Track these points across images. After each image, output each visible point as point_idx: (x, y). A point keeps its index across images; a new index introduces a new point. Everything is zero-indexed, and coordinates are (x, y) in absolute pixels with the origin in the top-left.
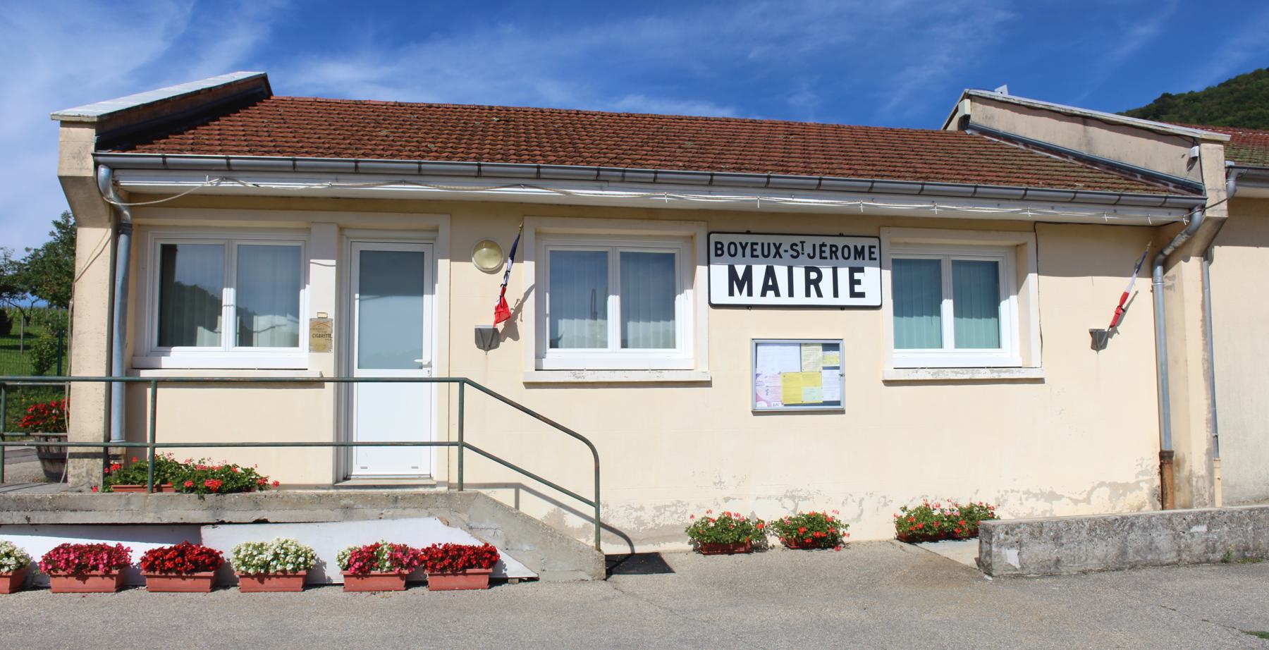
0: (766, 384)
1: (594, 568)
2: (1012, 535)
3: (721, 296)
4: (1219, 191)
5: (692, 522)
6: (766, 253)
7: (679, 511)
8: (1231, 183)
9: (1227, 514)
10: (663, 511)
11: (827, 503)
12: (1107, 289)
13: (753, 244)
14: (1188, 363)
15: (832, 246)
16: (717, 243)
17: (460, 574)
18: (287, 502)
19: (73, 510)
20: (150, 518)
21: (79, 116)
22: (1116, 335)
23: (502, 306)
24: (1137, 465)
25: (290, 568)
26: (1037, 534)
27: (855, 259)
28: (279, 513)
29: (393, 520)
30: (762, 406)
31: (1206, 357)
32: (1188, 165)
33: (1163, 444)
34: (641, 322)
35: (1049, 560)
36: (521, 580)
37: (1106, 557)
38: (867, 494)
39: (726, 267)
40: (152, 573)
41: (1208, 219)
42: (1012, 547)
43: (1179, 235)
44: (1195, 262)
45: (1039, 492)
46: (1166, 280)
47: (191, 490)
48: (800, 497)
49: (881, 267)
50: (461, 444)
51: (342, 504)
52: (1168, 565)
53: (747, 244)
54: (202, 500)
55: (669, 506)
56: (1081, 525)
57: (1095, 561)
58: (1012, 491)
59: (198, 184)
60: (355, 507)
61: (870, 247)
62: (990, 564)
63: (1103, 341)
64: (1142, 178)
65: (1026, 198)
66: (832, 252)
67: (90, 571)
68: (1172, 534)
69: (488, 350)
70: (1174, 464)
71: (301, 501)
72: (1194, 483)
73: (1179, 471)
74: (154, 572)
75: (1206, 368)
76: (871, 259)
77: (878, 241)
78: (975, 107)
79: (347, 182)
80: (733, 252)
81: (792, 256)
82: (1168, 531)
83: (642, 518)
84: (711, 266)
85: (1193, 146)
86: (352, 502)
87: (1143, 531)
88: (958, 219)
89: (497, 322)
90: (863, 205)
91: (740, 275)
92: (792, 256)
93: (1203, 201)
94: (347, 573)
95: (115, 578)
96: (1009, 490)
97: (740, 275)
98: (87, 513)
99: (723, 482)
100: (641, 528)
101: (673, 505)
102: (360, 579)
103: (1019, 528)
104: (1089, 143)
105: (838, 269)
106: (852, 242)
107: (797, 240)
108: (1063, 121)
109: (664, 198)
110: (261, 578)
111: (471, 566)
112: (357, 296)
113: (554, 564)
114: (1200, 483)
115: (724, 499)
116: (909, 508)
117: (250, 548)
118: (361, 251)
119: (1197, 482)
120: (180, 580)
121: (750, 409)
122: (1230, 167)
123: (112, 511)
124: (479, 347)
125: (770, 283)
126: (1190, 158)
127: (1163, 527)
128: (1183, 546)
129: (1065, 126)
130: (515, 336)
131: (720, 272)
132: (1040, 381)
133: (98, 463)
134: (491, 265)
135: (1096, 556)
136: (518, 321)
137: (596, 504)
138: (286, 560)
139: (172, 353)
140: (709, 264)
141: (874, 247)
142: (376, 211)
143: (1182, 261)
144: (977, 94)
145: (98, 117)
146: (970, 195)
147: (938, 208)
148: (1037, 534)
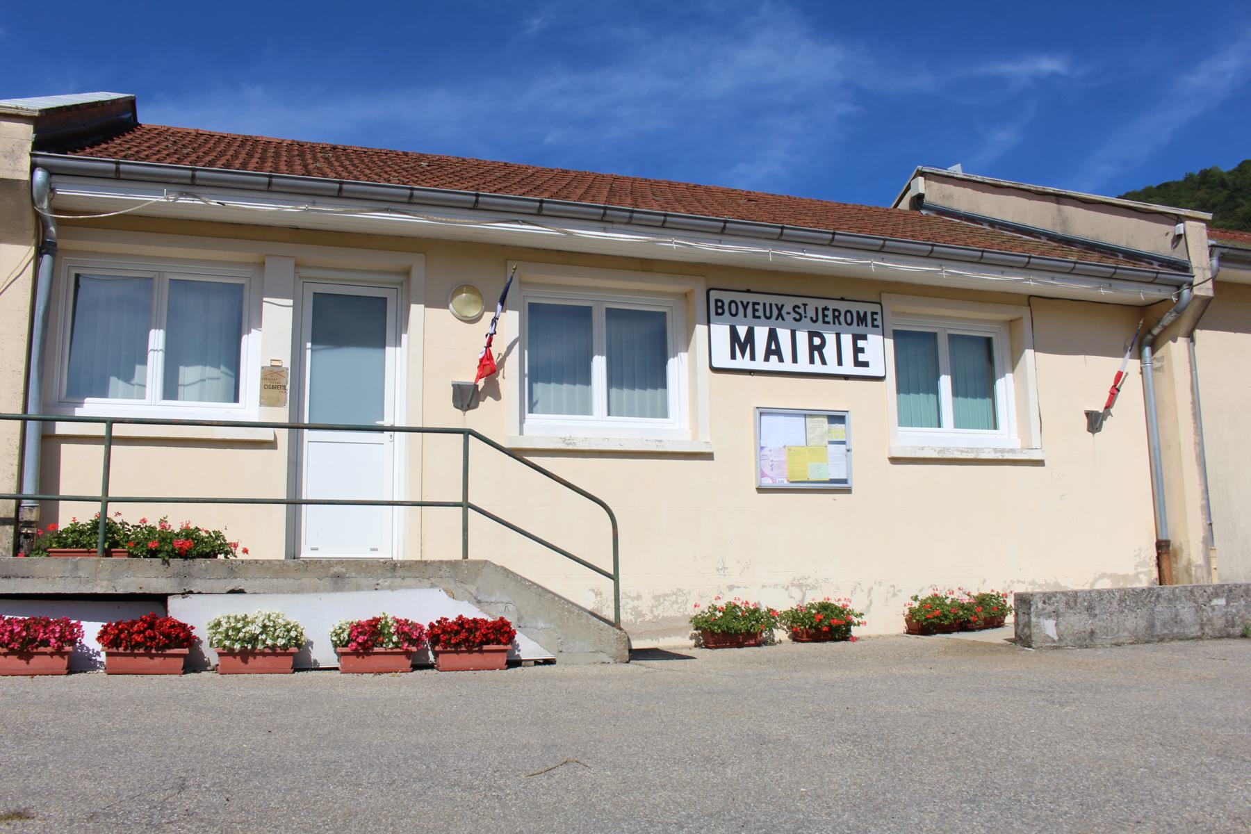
0: (771, 459)
1: (616, 648)
2: (1049, 605)
3: (722, 358)
4: (1204, 269)
5: (698, 611)
6: (768, 315)
7: (680, 601)
8: (1215, 262)
9: (1243, 588)
10: (662, 600)
11: (835, 592)
12: (1101, 368)
13: (754, 304)
14: (1182, 447)
15: (834, 310)
16: (717, 301)
17: (476, 651)
18: (268, 569)
19: (6, 577)
20: (102, 587)
21: (17, 108)
22: (1109, 417)
23: (488, 357)
24: (1136, 556)
25: (282, 643)
26: (1072, 604)
27: (858, 325)
28: (258, 582)
29: (393, 590)
30: (767, 482)
31: (1197, 441)
32: (1173, 243)
33: (1159, 532)
34: (625, 390)
35: (1084, 632)
36: (537, 663)
37: (1136, 629)
38: (875, 582)
39: (727, 328)
40: (114, 650)
41: (1196, 297)
42: (1050, 617)
43: (1168, 314)
44: (1182, 342)
45: (1044, 583)
46: (1154, 362)
47: (153, 554)
48: (808, 585)
49: (883, 335)
50: (466, 505)
51: (332, 572)
52: (1192, 639)
53: (748, 303)
54: (166, 566)
55: (668, 595)
56: (1112, 595)
57: (1126, 634)
58: (1019, 581)
59: (153, 199)
60: (347, 575)
61: (873, 313)
62: (1030, 636)
63: (1099, 423)
64: (1123, 257)
65: (1029, 266)
66: (834, 317)
67: (37, 647)
68: (1195, 607)
69: (466, 411)
70: (1171, 555)
71: (285, 568)
72: (1193, 573)
73: (1176, 562)
74: (117, 649)
75: (1198, 452)
76: (873, 326)
77: (880, 308)
78: (930, 186)
79: (332, 207)
80: (734, 312)
81: (795, 319)
82: (1192, 604)
83: (639, 609)
84: (712, 325)
85: (1177, 224)
86: (344, 570)
87: (1168, 603)
88: (955, 288)
89: (479, 377)
90: (875, 266)
91: (742, 337)
92: (795, 319)
93: (1191, 279)
94: (340, 649)
95: (66, 657)
96: (1014, 580)
97: (742, 337)
98: (23, 580)
99: (727, 568)
100: (639, 620)
101: (673, 594)
102: (361, 658)
103: (1056, 597)
104: (1064, 222)
105: (842, 335)
106: (854, 307)
107: (799, 301)
108: (1033, 200)
109: (672, 245)
110: (245, 655)
111: (487, 643)
112: (309, 345)
113: (572, 645)
114: (1199, 574)
115: (728, 587)
116: (920, 598)
117: (232, 620)
118: (314, 293)
119: (1195, 571)
120: (147, 658)
121: (754, 486)
122: (1212, 246)
123: (54, 578)
124: (456, 406)
125: (773, 347)
126: (1175, 236)
127: (1187, 599)
128: (1205, 619)
129: (1036, 205)
130: (497, 396)
131: (721, 332)
132: (1040, 463)
133: (7, 531)
134: (473, 313)
135: (1128, 629)
136: (500, 378)
137: (615, 577)
138: (276, 634)
139: (85, 404)
140: (709, 323)
141: (877, 313)
142: (341, 246)
143: (1170, 342)
144: (932, 171)
145: (40, 111)
146: (976, 260)
147: (946, 272)
148: (1072, 604)
